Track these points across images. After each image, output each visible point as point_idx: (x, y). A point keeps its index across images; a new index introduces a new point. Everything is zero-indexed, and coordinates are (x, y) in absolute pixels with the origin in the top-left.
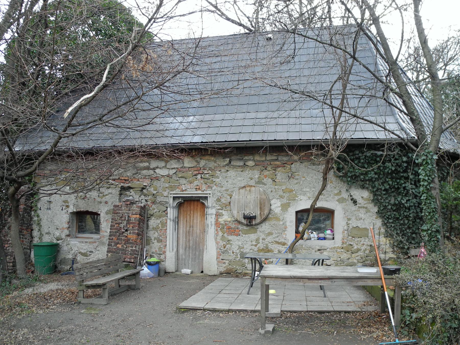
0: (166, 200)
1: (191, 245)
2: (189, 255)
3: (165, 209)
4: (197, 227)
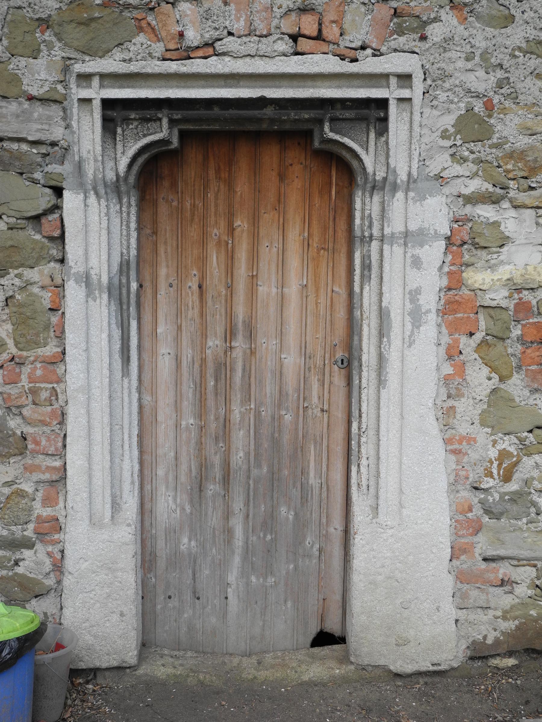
0: (42, 124)
1: (238, 457)
2: (229, 532)
3: (46, 198)
4: (281, 334)
